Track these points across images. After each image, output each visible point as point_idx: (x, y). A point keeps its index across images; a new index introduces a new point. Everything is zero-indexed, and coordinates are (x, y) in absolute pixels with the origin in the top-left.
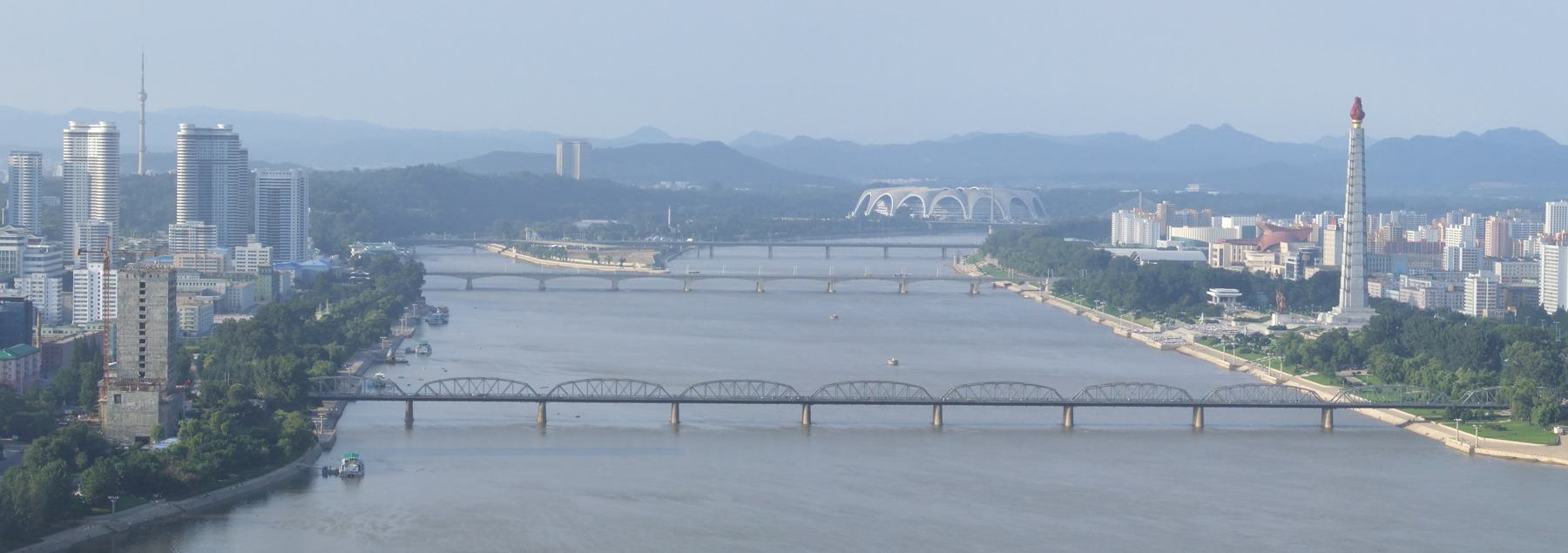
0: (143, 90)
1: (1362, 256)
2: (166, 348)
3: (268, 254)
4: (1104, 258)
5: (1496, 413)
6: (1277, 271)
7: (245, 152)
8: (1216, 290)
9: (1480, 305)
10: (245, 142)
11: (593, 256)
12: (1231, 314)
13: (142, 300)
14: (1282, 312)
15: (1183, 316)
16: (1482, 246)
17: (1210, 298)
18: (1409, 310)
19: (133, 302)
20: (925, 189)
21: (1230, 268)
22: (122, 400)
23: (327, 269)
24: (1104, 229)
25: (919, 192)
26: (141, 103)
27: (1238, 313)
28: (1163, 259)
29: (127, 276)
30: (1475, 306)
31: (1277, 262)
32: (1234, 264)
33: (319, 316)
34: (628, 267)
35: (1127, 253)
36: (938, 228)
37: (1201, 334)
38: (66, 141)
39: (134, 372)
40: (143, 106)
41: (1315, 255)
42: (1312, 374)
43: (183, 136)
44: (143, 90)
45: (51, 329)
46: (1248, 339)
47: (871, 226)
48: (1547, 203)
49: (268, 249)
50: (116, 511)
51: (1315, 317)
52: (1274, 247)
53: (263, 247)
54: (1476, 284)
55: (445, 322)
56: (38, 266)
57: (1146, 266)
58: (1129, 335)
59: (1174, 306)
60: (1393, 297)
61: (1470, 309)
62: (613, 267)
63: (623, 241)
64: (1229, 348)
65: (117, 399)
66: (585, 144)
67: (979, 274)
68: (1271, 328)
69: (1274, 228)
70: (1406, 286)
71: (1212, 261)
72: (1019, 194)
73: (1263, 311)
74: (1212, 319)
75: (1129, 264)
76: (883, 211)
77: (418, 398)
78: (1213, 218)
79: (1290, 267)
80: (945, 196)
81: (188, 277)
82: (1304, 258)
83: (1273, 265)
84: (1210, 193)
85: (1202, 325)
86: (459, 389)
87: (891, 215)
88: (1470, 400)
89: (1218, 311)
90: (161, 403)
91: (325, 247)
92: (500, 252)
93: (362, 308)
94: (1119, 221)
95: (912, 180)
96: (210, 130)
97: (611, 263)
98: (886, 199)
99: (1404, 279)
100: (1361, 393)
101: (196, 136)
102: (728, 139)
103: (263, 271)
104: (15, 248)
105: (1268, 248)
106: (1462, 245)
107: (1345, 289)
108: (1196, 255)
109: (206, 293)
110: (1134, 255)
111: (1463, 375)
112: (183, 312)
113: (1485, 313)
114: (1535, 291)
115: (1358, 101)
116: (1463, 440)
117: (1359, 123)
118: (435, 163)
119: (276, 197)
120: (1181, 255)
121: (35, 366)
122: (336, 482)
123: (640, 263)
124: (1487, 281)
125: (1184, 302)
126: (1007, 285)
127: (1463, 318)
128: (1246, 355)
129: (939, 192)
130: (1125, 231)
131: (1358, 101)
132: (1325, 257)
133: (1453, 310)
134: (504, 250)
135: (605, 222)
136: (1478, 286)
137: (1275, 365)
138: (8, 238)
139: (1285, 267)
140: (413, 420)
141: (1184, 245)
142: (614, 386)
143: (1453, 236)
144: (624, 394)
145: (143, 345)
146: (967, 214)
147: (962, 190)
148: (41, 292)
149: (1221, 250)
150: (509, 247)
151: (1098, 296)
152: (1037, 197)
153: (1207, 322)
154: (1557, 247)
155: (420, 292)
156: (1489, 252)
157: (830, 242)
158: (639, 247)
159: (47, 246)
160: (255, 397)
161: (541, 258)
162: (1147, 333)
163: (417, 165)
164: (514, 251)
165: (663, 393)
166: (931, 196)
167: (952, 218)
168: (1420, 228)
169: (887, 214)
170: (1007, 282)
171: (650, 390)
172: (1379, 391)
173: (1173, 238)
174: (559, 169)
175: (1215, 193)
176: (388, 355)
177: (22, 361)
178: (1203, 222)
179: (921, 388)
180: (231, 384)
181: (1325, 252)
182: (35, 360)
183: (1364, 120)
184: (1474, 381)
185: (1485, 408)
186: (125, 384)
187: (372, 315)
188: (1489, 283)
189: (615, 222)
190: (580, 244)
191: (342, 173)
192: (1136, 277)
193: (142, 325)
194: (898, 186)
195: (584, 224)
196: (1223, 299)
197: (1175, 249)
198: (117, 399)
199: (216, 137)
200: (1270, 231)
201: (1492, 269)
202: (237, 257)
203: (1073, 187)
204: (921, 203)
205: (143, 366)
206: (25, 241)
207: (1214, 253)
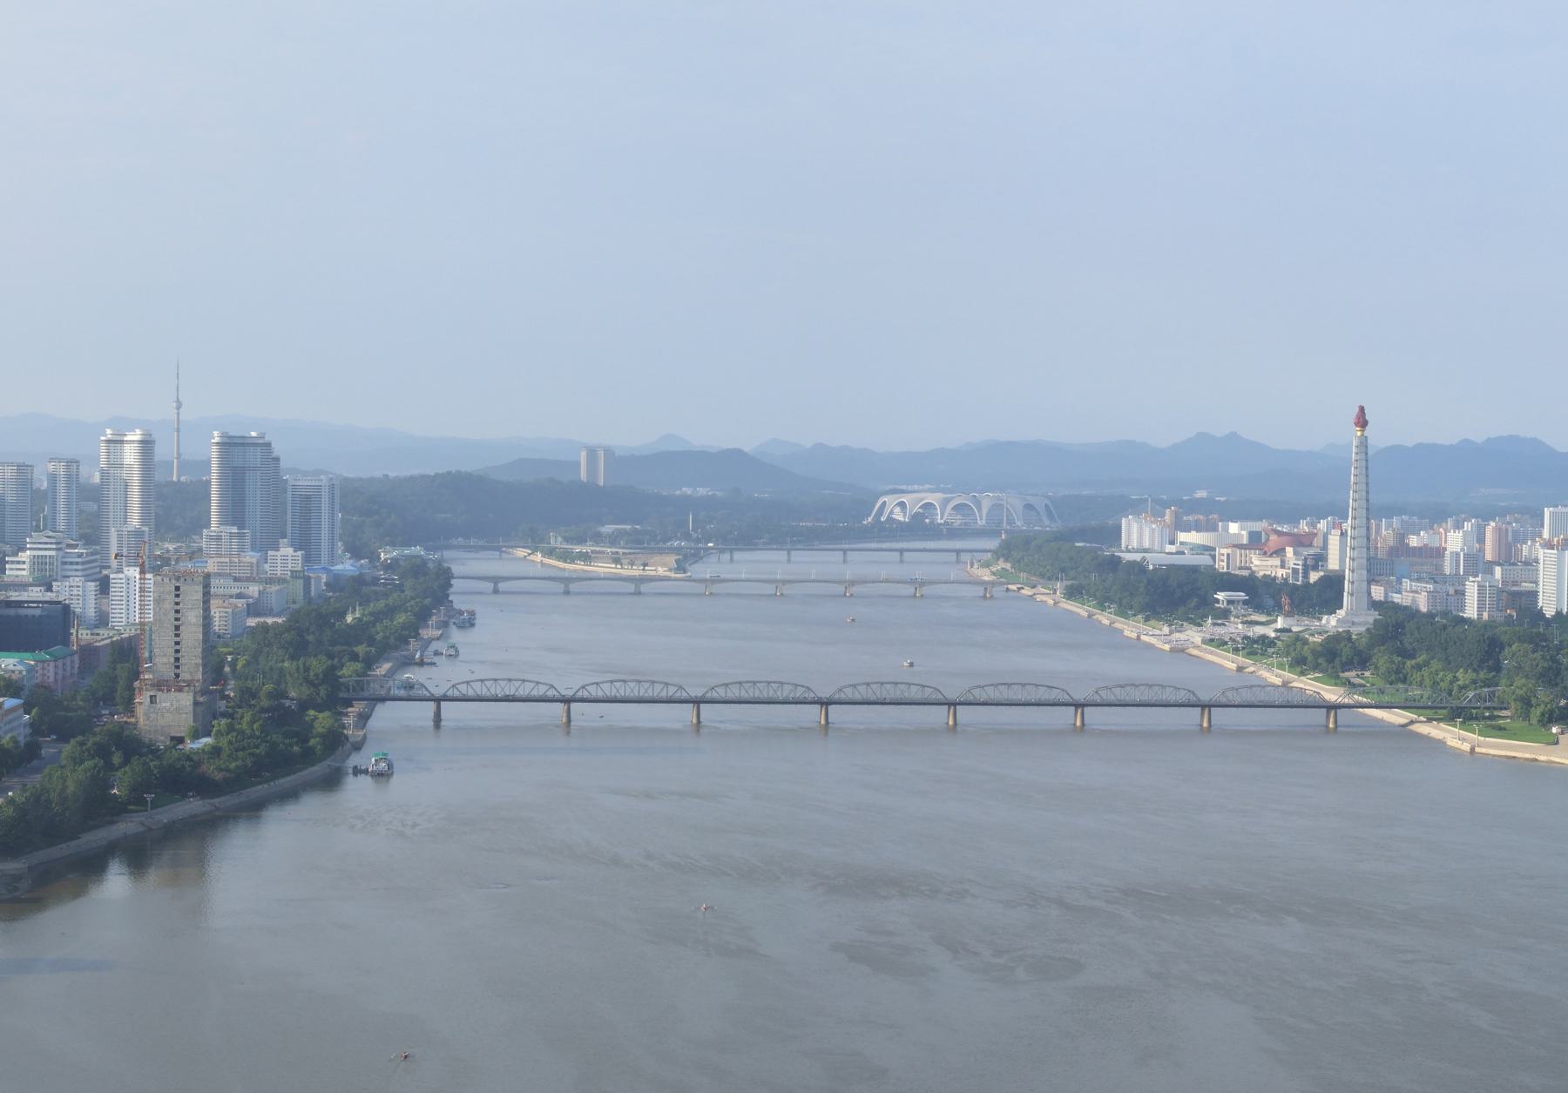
0: (178, 399)
1: (1365, 560)
2: (200, 650)
3: (300, 558)
4: (1115, 563)
5: (1496, 713)
7: (277, 459)
8: (1223, 594)
9: (1480, 608)
10: (277, 449)
11: (617, 561)
12: (1238, 617)
13: (177, 604)
14: (1288, 615)
15: (1191, 619)
16: (1482, 550)
17: (1217, 601)
18: (1411, 613)
19: (168, 605)
20: (940, 495)
21: (1238, 572)
22: (158, 701)
23: (358, 573)
25: (934, 498)
27: (1244, 616)
28: (1171, 563)
29: (163, 580)
30: (1476, 609)
31: (1283, 566)
32: (1241, 568)
33: (349, 619)
34: (650, 571)
35: (1137, 557)
36: (953, 533)
38: (103, 447)
39: (169, 673)
40: (178, 414)
41: (1319, 559)
42: (1317, 675)
45: (89, 632)
46: (1255, 641)
47: (889, 531)
48: (1546, 509)
49: (299, 553)
50: (152, 809)
52: (1280, 552)
53: (295, 551)
54: (1476, 588)
56: (76, 570)
57: (1155, 570)
59: (1181, 610)
60: (1396, 600)
61: (1471, 612)
62: (636, 571)
63: (645, 545)
64: (1236, 650)
65: (153, 699)
66: (609, 452)
67: (993, 578)
68: (1277, 630)
71: (1219, 565)
73: (1269, 614)
74: (1219, 622)
75: (1139, 568)
76: (899, 516)
78: (1220, 524)
79: (1295, 571)
81: (222, 581)
82: (1309, 562)
84: (1217, 499)
85: (1210, 628)
86: (486, 690)
87: (907, 520)
89: (1225, 614)
90: (196, 703)
91: (356, 552)
92: (525, 556)
93: (391, 611)
94: (1129, 525)
95: (927, 486)
96: (244, 437)
97: (634, 567)
98: (902, 505)
99: (1406, 583)
101: (229, 443)
103: (295, 575)
104: (53, 553)
106: (1463, 550)
108: (1204, 560)
109: (240, 596)
110: (1144, 559)
111: (1463, 677)
112: (217, 615)
113: (1485, 616)
114: (1533, 595)
115: (1362, 409)
116: (1464, 740)
117: (1363, 431)
119: (307, 503)
120: (1189, 559)
121: (72, 668)
122: (364, 781)
125: (1193, 604)
126: (1019, 589)
127: (1463, 620)
128: (1252, 657)
129: (952, 498)
131: (1362, 409)
132: (1329, 561)
134: (529, 554)
135: (628, 527)
137: (1281, 666)
138: (46, 543)
141: (1192, 549)
144: (646, 695)
145: (178, 647)
146: (981, 519)
147: (975, 496)
148: (79, 595)
149: (1228, 555)
150: (535, 550)
153: (1215, 624)
154: (1555, 551)
155: (448, 595)
158: (661, 551)
159: (85, 551)
160: (287, 698)
161: (566, 562)
162: (1157, 635)
164: (540, 556)
165: (684, 694)
166: (946, 502)
167: (966, 524)
169: (902, 519)
170: (1020, 586)
172: (1382, 692)
173: (1182, 543)
174: (583, 476)
177: (60, 663)
178: (1212, 528)
182: (72, 662)
184: (1474, 682)
185: (1485, 708)
186: (160, 685)
188: (1490, 586)
189: (638, 527)
190: (604, 549)
192: (1145, 581)
194: (912, 492)
195: (608, 529)
196: (1230, 602)
197: (1183, 553)
198: (153, 699)
199: (249, 445)
201: (1492, 573)
205: (177, 667)
206: (63, 546)
207: (1222, 557)
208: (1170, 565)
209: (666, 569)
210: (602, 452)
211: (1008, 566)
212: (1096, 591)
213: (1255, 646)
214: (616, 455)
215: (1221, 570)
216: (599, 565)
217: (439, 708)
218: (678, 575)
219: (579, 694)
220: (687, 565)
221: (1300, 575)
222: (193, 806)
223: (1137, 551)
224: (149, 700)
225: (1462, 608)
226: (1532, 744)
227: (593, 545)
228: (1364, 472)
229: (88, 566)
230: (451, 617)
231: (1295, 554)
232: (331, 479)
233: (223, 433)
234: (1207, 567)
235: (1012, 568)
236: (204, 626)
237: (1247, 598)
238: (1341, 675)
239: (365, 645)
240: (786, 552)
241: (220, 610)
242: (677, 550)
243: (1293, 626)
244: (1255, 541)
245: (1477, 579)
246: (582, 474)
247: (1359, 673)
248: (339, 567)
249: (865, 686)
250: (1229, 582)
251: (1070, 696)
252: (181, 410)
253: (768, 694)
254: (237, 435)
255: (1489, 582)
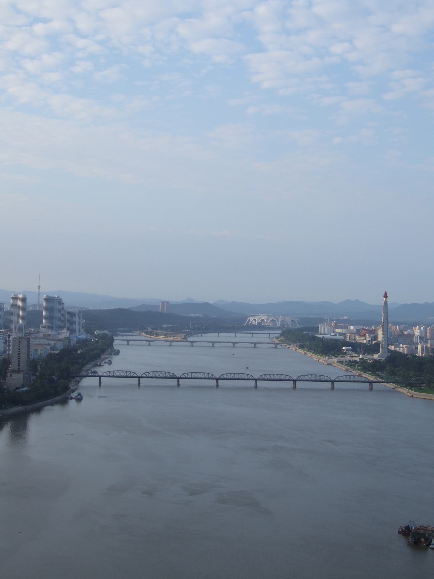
0: (39, 285)
3: (68, 333)
4: (314, 338)
5: (421, 385)
6: (365, 342)
8: (345, 348)
9: (422, 353)
10: (64, 301)
12: (349, 355)
14: (363, 354)
15: (335, 355)
16: (426, 335)
17: (343, 350)
18: (400, 354)
20: (266, 317)
21: (352, 341)
23: (86, 338)
24: (316, 330)
25: (264, 318)
26: (38, 289)
27: (351, 354)
28: (331, 338)
29: (15, 339)
31: (365, 340)
33: (79, 352)
34: (176, 338)
36: (269, 328)
37: (339, 360)
38: (11, 299)
39: (16, 368)
40: (39, 290)
41: (376, 338)
42: (369, 372)
43: (45, 299)
44: (39, 285)
47: (250, 328)
49: (68, 332)
50: (5, 409)
51: (80, 352)
52: (364, 335)
53: (67, 331)
54: (421, 347)
55: (118, 354)
57: (326, 340)
58: (318, 361)
60: (397, 350)
61: (419, 354)
62: (171, 339)
64: (346, 365)
65: (11, 376)
66: (168, 303)
68: (360, 359)
69: (365, 329)
70: (401, 347)
71: (347, 339)
72: (294, 319)
73: (358, 354)
74: (343, 356)
75: (321, 339)
76: (254, 323)
77: (141, 377)
78: (349, 326)
79: (369, 341)
80: (272, 319)
81: (44, 340)
82: (373, 338)
83: (364, 340)
84: (350, 319)
85: (340, 358)
86: (115, 374)
87: (256, 324)
88: (413, 381)
89: (345, 354)
90: (24, 377)
92: (140, 334)
94: (321, 327)
95: (265, 314)
96: (53, 297)
97: (171, 337)
99: (401, 345)
100: (382, 378)
101: (49, 299)
102: (211, 302)
103: (66, 338)
105: (363, 335)
106: (419, 335)
107: (381, 348)
108: (342, 337)
109: (48, 345)
110: (323, 337)
112: (40, 350)
113: (424, 355)
115: (386, 293)
116: (410, 393)
117: (386, 299)
118: (123, 308)
119: (72, 317)
120: (338, 337)
122: (74, 401)
123: (179, 337)
124: (424, 346)
126: (286, 345)
127: (416, 356)
129: (271, 318)
130: (323, 330)
131: (386, 293)
133: (414, 354)
135: (171, 325)
136: (422, 347)
137: (359, 370)
139: (367, 341)
140: (101, 383)
141: (339, 334)
142: (126, 373)
143: (417, 332)
145: (19, 360)
146: (278, 324)
149: (349, 336)
150: (142, 332)
151: (311, 349)
152: (299, 319)
153: (342, 357)
155: (113, 345)
156: (428, 337)
157: (236, 332)
159: (3, 330)
160: (54, 376)
163: (117, 308)
164: (144, 333)
165: (136, 375)
166: (267, 319)
168: (408, 330)
170: (286, 344)
171: (249, 376)
172: (388, 378)
173: (336, 332)
174: (160, 310)
175: (352, 319)
176: (99, 364)
178: (346, 327)
179: (289, 376)
180: (48, 371)
181: (379, 337)
183: (387, 298)
185: (418, 383)
186: (14, 371)
187: (96, 352)
189: (174, 325)
190: (163, 332)
191: (96, 310)
193: (19, 354)
194: (258, 316)
195: (165, 326)
198: (11, 376)
199: (55, 299)
200: (364, 331)
201: (427, 343)
202: (59, 334)
203: (312, 317)
204: (265, 321)
205: (19, 366)
207: (347, 337)
208: (330, 339)
209: (180, 338)
210: (166, 303)
211: (283, 338)
212: (308, 346)
213: (352, 363)
214: (170, 304)
215: (347, 340)
216: (161, 336)
217: (139, 381)
218: (183, 340)
219: (143, 376)
220: (187, 337)
221: (370, 342)
222: (19, 408)
223: (322, 334)
224: (9, 376)
225: (417, 353)
226: (430, 394)
227: (160, 331)
228: (386, 312)
229: (4, 335)
230: (113, 352)
231: (369, 336)
232: (79, 310)
233: (14, 295)
234: (343, 339)
235: (284, 339)
236: (27, 353)
237: (352, 349)
238: (376, 373)
239: (82, 360)
240: (235, 334)
241: (41, 349)
242: (184, 332)
243: (364, 358)
244: (358, 332)
245: (421, 344)
246: (160, 309)
247: (382, 372)
248: (80, 336)
249: (230, 374)
250: (347, 344)
251: (137, 375)
252: (40, 289)
253: (230, 377)
254: (51, 296)
255: (425, 345)
